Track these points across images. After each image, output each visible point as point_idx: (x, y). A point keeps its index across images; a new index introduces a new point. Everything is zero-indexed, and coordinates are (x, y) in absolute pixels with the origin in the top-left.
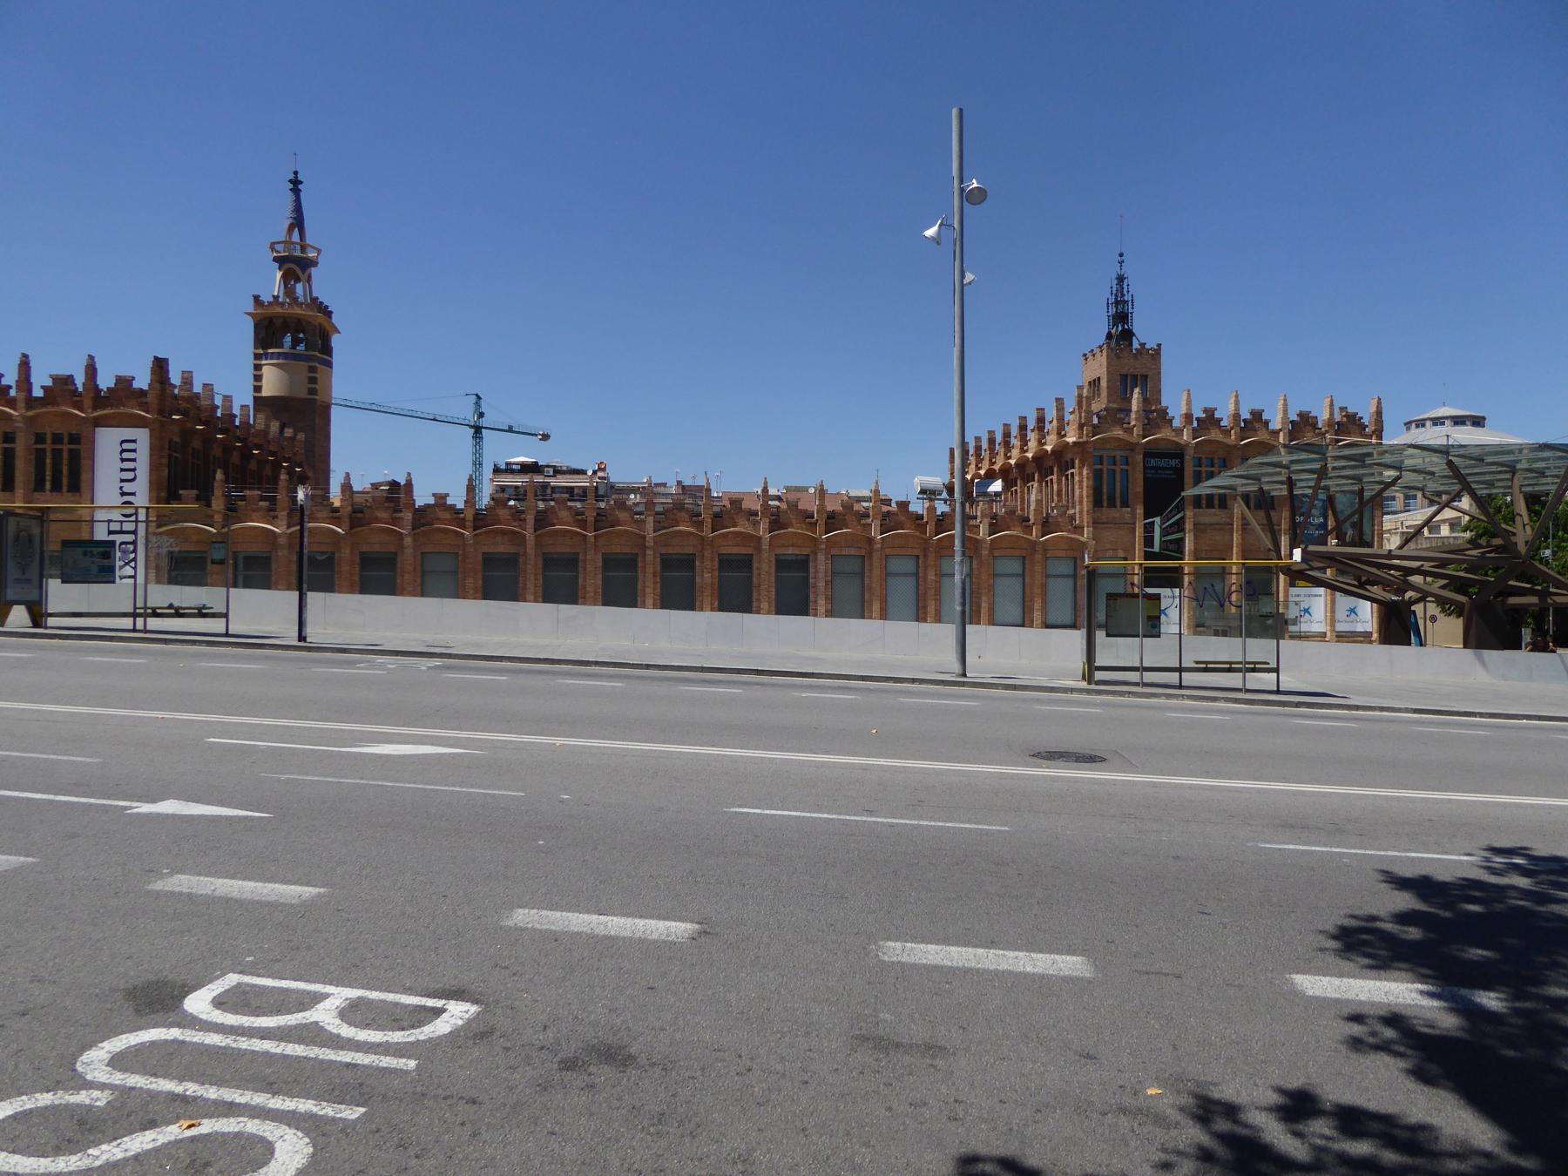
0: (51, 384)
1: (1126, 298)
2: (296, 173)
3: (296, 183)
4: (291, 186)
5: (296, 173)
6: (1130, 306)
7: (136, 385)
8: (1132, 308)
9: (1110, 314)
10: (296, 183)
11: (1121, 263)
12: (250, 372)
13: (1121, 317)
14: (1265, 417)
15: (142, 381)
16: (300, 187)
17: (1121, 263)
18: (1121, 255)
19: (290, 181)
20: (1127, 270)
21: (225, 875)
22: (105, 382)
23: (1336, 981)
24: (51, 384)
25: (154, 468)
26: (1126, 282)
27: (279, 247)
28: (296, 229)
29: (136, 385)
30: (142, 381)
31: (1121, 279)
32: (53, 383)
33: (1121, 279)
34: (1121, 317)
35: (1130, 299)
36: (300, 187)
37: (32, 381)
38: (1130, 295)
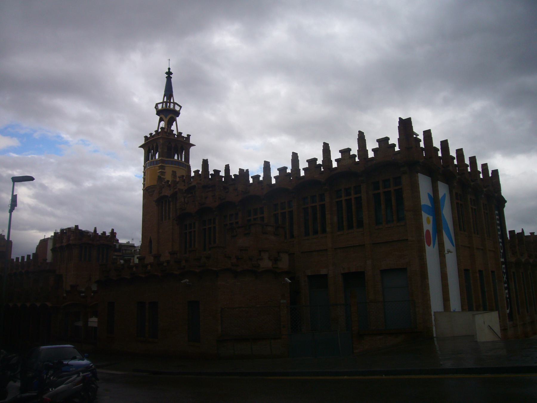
2: (169, 69)
3: (169, 73)
5: (169, 69)
10: (169, 73)
27: (160, 107)
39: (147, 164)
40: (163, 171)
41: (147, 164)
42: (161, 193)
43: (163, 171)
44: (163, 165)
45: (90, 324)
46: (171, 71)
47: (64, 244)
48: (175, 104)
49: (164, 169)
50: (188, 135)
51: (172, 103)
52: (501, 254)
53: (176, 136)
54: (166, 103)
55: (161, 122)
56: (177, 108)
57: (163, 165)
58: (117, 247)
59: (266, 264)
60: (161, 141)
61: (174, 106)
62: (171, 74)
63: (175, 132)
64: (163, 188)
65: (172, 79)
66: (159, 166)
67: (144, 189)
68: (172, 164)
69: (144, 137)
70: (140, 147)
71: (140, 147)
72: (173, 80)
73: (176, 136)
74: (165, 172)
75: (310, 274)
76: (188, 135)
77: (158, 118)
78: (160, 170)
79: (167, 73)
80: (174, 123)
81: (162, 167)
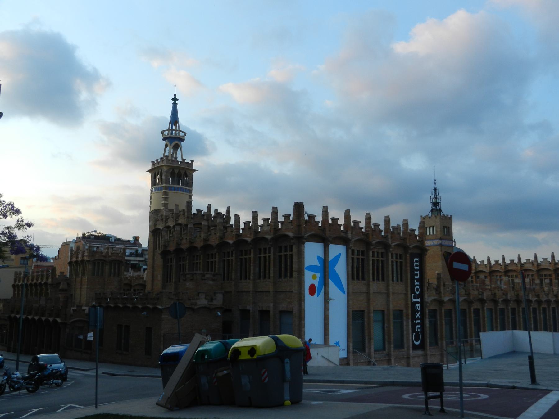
0: (196, 213)
1: (438, 197)
2: (175, 95)
3: (175, 100)
4: (173, 102)
5: (175, 95)
6: (439, 200)
7: (515, 262)
8: (440, 201)
9: (432, 202)
10: (175, 100)
11: (435, 183)
12: (443, 212)
13: (436, 204)
14: (481, 261)
15: (516, 261)
16: (177, 102)
17: (435, 183)
18: (435, 180)
19: (172, 99)
20: (438, 186)
21: (161, 226)
22: (507, 261)
23: (484, 415)
24: (196, 213)
25: (356, 381)
26: (437, 190)
27: (166, 133)
28: (320, 266)
29: (515, 262)
30: (516, 261)
31: (435, 189)
32: (284, 219)
33: (435, 189)
34: (436, 204)
35: (439, 197)
36: (177, 102)
37: (505, 261)
38: (439, 195)
39: (153, 188)
40: (166, 196)
41: (153, 188)
42: (156, 225)
43: (166, 196)
44: (166, 191)
45: (88, 339)
46: (177, 97)
47: (79, 259)
48: (180, 131)
49: (168, 195)
50: (191, 161)
51: (177, 130)
52: (416, 295)
53: (179, 163)
54: (172, 130)
55: (166, 148)
56: (182, 134)
57: (166, 191)
58: (140, 251)
59: (202, 302)
60: (165, 169)
61: (179, 134)
62: (177, 100)
63: (179, 159)
64: (158, 220)
65: (177, 105)
66: (163, 192)
67: (151, 211)
68: (175, 190)
69: (151, 162)
70: (147, 171)
71: (147, 171)
72: (178, 107)
73: (179, 163)
74: (168, 198)
75: (241, 309)
76: (191, 161)
77: (164, 143)
78: (164, 196)
79: (172, 99)
80: (179, 149)
81: (165, 194)
